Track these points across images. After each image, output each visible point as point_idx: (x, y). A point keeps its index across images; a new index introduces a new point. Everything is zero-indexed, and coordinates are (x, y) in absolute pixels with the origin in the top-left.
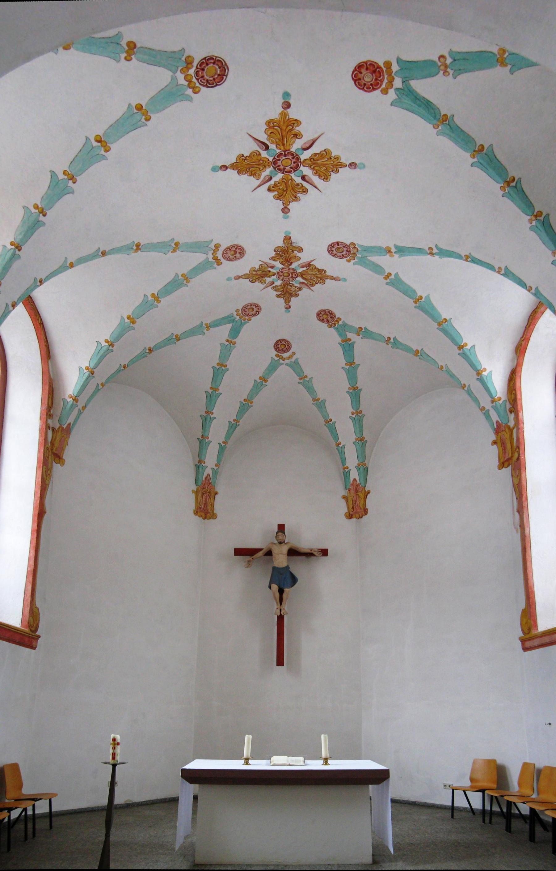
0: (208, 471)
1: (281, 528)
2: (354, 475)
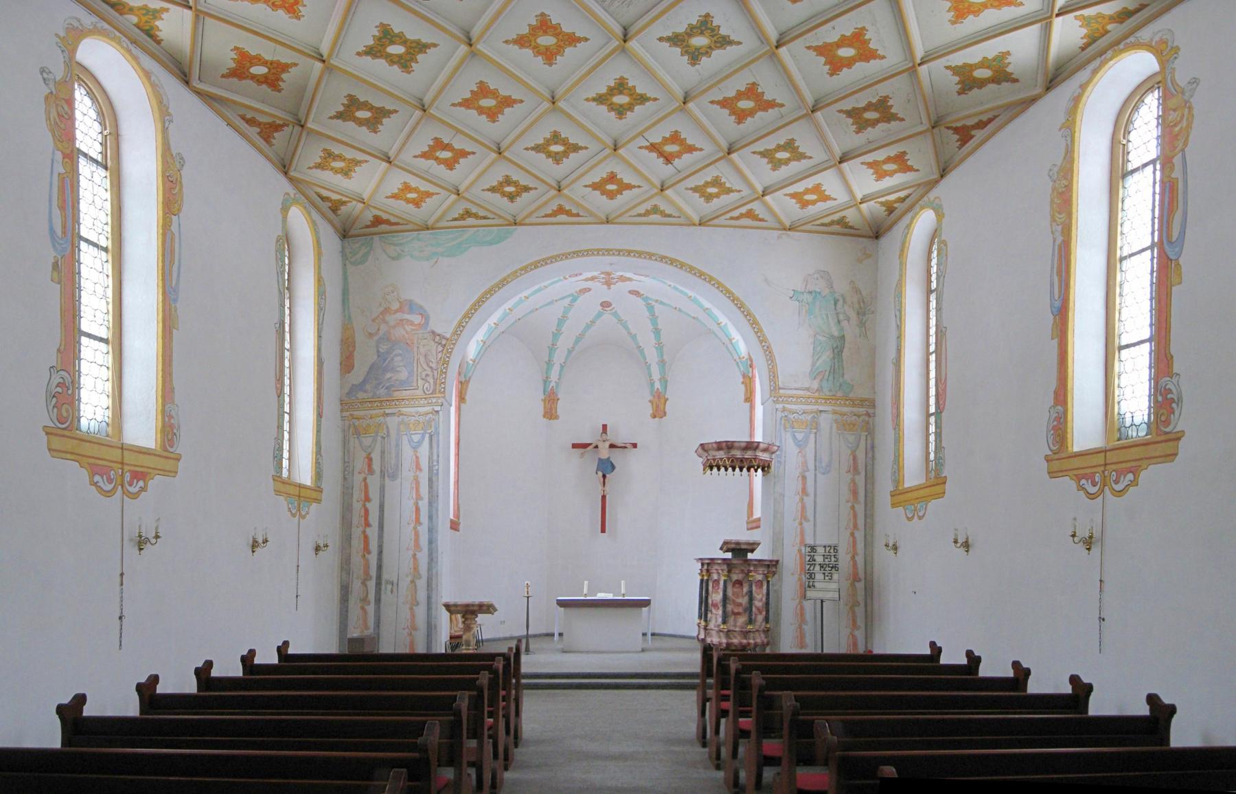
0: (553, 384)
1: (605, 427)
2: (657, 385)
